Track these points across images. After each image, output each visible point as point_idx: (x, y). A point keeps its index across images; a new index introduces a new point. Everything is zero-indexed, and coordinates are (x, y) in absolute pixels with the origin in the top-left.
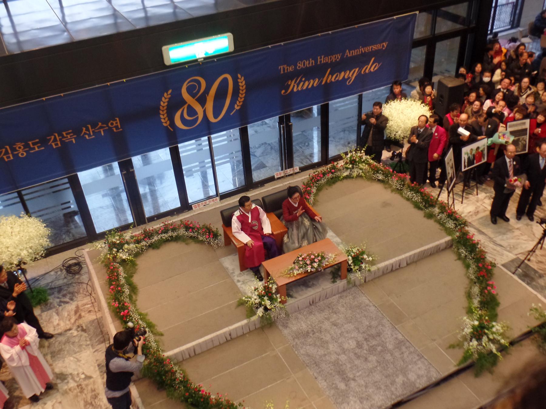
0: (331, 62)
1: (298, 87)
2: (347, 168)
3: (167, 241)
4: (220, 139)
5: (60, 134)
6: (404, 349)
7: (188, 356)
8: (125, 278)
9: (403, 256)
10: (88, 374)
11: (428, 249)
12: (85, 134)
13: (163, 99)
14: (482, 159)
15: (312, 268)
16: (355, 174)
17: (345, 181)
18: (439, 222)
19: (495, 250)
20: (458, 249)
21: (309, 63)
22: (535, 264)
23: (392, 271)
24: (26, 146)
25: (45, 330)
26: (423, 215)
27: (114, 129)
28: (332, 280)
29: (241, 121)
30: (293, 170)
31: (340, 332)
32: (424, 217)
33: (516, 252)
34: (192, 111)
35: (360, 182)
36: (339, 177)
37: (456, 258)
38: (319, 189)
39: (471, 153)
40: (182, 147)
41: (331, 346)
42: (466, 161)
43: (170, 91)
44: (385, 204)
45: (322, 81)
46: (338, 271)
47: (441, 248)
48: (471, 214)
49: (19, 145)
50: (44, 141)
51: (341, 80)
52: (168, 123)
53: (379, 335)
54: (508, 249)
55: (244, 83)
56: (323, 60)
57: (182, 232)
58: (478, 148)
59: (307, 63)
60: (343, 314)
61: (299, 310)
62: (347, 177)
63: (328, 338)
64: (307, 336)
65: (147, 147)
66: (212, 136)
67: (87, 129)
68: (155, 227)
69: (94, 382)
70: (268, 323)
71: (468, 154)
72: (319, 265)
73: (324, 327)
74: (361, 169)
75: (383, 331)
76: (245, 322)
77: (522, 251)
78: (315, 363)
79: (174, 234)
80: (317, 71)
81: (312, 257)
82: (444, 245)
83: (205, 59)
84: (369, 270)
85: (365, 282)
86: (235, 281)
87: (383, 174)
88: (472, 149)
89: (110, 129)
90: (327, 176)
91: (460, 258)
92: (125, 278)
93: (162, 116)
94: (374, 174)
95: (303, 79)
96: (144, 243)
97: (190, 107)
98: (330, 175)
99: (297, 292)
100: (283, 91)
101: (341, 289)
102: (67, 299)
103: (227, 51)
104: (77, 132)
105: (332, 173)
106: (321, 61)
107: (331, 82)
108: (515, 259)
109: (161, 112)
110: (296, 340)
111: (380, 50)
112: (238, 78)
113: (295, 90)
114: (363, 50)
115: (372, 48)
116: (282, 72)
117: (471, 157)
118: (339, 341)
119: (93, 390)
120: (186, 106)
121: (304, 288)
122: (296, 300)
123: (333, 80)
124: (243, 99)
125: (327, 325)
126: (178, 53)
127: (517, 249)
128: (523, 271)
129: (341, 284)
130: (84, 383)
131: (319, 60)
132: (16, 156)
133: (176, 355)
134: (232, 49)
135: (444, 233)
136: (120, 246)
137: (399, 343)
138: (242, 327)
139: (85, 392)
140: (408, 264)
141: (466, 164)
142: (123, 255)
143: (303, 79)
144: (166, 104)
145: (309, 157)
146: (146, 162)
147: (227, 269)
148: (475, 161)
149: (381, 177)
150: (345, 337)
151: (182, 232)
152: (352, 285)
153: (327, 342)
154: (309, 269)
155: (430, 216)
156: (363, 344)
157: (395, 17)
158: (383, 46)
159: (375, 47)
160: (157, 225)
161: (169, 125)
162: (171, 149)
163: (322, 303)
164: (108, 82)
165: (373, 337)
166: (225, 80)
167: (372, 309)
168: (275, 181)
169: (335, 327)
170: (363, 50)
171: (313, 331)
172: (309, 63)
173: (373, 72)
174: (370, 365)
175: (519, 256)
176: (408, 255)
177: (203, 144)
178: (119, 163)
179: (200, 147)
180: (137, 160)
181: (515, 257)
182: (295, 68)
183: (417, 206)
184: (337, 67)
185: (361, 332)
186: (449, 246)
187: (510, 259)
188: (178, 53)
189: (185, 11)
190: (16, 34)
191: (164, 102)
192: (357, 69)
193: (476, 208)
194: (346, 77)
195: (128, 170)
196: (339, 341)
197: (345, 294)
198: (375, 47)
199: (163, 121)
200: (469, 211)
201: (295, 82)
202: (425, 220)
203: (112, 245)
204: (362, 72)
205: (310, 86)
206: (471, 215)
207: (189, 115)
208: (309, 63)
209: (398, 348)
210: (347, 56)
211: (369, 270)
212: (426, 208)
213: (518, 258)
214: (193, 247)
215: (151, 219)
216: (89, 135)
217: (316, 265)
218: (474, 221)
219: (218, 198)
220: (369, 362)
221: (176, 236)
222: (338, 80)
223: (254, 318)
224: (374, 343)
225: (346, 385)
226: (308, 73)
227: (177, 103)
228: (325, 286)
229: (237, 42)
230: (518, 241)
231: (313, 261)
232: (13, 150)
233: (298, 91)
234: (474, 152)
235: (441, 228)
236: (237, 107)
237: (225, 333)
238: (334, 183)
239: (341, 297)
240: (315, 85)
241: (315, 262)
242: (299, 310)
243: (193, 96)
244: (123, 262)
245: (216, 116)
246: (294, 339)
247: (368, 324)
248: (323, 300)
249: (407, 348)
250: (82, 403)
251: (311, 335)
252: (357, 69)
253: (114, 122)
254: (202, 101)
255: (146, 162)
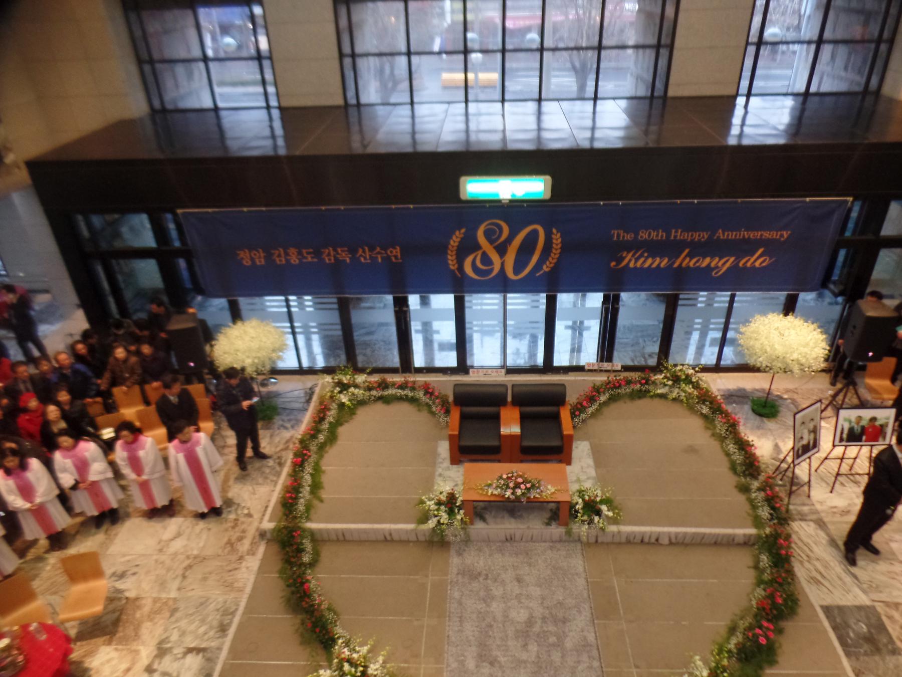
0: (699, 240)
1: (636, 262)
2: (665, 385)
3: (400, 399)
4: (517, 301)
5: (335, 250)
6: (585, 658)
7: (335, 538)
8: (330, 423)
9: (666, 529)
10: (252, 512)
11: (710, 534)
12: (361, 256)
13: (454, 238)
14: (881, 439)
15: (512, 494)
16: (674, 395)
17: (657, 400)
18: (751, 501)
19: (840, 579)
20: (760, 553)
21: (657, 236)
22: (898, 628)
23: (715, 543)
24: (300, 253)
25: (262, 450)
26: (735, 484)
27: (393, 259)
28: (546, 521)
29: (551, 285)
30: (613, 366)
31: (518, 592)
32: (736, 487)
33: (876, 596)
34: (486, 260)
35: (677, 407)
36: (649, 391)
37: (751, 564)
38: (613, 399)
39: (858, 423)
40: (740, 296)
41: (494, 605)
42: (846, 432)
43: (463, 230)
44: (691, 450)
45: (674, 263)
46: (559, 513)
47: (736, 541)
48: (835, 510)
49: (292, 251)
50: (317, 253)
51: (703, 268)
52: (456, 266)
53: (565, 621)
54: (865, 586)
55: (560, 240)
56: (678, 234)
57: (420, 394)
58: (874, 419)
59: (654, 234)
60: (539, 570)
61: (488, 541)
62: (663, 396)
63: (497, 591)
64: (476, 578)
65: (427, 289)
66: (509, 295)
67: (364, 252)
68: (395, 380)
69: (251, 523)
70: (438, 542)
71: (850, 422)
72: (523, 494)
73: (504, 576)
74: (685, 392)
75: (575, 619)
76: (411, 526)
77: (888, 600)
78: (460, 617)
79: (410, 394)
80: (671, 248)
81: (520, 480)
82: (741, 541)
83: (511, 201)
84: (602, 529)
85: (597, 541)
86: (437, 473)
87: (710, 408)
88: (860, 417)
89: (388, 258)
90: (632, 387)
91: (756, 567)
92: (330, 423)
93: (449, 257)
94: (698, 403)
95: (646, 255)
96: (374, 393)
97: (484, 254)
98: (639, 386)
99: (495, 517)
100: (613, 264)
101: (556, 537)
102: (288, 425)
103: (541, 197)
104: (353, 251)
105: (642, 384)
106: (675, 237)
107: (688, 267)
108: (868, 607)
109: (449, 252)
110: (460, 577)
111: (776, 240)
112: (552, 233)
113: (632, 265)
114: (745, 234)
115: (762, 235)
116: (615, 238)
117: (858, 429)
118: (509, 604)
119: (244, 531)
120: (480, 253)
121: (506, 515)
122: (486, 526)
123: (691, 264)
124: (555, 261)
125: (508, 576)
126: (476, 188)
127: (881, 592)
128: (869, 631)
129: (556, 530)
130: (242, 519)
131: (673, 234)
132: (288, 261)
133: (320, 530)
134: (548, 196)
135: (749, 521)
136: (344, 387)
137: (584, 646)
138: (407, 531)
139: (237, 529)
140: (671, 543)
141: (845, 436)
142: (344, 399)
143: (646, 255)
144: (456, 244)
145: (647, 356)
146: (425, 302)
147: (439, 455)
148: (864, 438)
149: (705, 410)
150: (520, 602)
151: (420, 394)
152: (570, 538)
153: (493, 598)
154: (508, 493)
155: (744, 489)
156: (536, 622)
157: (808, 199)
158: (782, 236)
159: (767, 235)
160: (421, 379)
161: (458, 269)
162: (456, 298)
163: (522, 544)
164: (245, 206)
165: (556, 621)
166: (535, 233)
167: (581, 582)
168: (584, 373)
169: (516, 583)
170: (745, 234)
171: (487, 575)
172: (657, 235)
173: (759, 269)
174: (524, 656)
175: (876, 604)
176: (673, 530)
177: (700, 299)
178: (394, 298)
179: (535, 304)
180: (414, 300)
181: (868, 603)
182: (636, 237)
183: (733, 468)
184: (698, 249)
185: (545, 605)
186: (747, 543)
187: (857, 603)
188: (476, 188)
189: (479, 142)
190: (741, 135)
191: (454, 241)
192: (732, 259)
193: (849, 505)
194: (713, 265)
195: (400, 308)
196: (509, 604)
197: (558, 545)
198: (767, 235)
199: (450, 262)
200: (834, 504)
201: (633, 256)
202: (735, 492)
203: (340, 384)
204: (741, 264)
205: (654, 266)
206: (835, 513)
207: (483, 263)
208: (657, 236)
209: (577, 651)
210: (718, 237)
211: (602, 529)
212: (745, 476)
213: (874, 607)
214: (424, 416)
215: (419, 370)
216: (365, 258)
217: (519, 492)
218: (834, 523)
219: (503, 371)
220: (527, 651)
221: (412, 397)
222: (699, 267)
223: (424, 527)
224: (550, 628)
225: (477, 666)
226: (654, 248)
227: (469, 246)
228: (534, 525)
229: (555, 189)
230: (892, 581)
231: (517, 486)
232: (287, 254)
233: (635, 268)
234: (864, 423)
235: (751, 512)
236: (545, 268)
237: (336, 530)
238: (640, 398)
239: (551, 548)
240: (662, 265)
241: (520, 488)
242: (488, 541)
243: (491, 242)
244: (342, 405)
245: (517, 271)
246: (458, 574)
247: (561, 598)
248: (527, 542)
249: (589, 657)
250: (225, 540)
251: (481, 579)
252: (732, 259)
253: (394, 251)
254: (502, 250)
255: (425, 302)
